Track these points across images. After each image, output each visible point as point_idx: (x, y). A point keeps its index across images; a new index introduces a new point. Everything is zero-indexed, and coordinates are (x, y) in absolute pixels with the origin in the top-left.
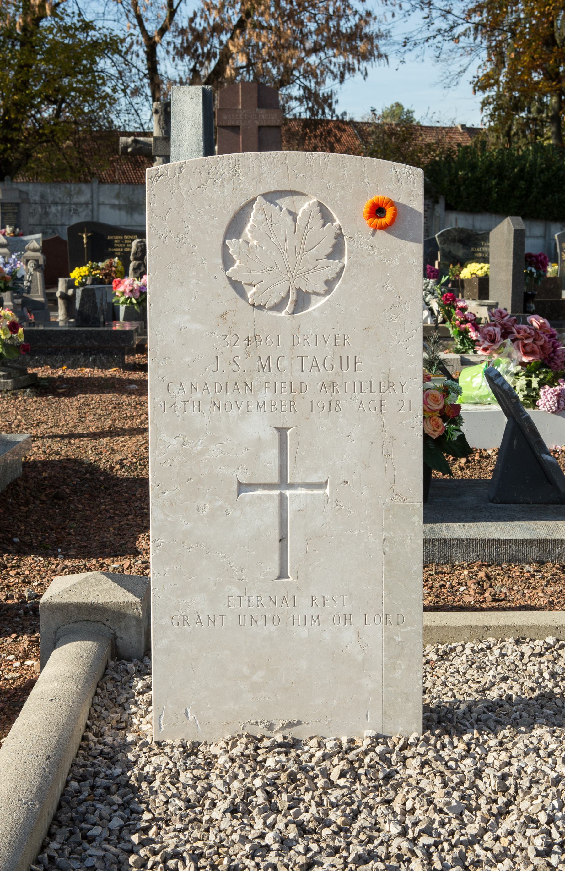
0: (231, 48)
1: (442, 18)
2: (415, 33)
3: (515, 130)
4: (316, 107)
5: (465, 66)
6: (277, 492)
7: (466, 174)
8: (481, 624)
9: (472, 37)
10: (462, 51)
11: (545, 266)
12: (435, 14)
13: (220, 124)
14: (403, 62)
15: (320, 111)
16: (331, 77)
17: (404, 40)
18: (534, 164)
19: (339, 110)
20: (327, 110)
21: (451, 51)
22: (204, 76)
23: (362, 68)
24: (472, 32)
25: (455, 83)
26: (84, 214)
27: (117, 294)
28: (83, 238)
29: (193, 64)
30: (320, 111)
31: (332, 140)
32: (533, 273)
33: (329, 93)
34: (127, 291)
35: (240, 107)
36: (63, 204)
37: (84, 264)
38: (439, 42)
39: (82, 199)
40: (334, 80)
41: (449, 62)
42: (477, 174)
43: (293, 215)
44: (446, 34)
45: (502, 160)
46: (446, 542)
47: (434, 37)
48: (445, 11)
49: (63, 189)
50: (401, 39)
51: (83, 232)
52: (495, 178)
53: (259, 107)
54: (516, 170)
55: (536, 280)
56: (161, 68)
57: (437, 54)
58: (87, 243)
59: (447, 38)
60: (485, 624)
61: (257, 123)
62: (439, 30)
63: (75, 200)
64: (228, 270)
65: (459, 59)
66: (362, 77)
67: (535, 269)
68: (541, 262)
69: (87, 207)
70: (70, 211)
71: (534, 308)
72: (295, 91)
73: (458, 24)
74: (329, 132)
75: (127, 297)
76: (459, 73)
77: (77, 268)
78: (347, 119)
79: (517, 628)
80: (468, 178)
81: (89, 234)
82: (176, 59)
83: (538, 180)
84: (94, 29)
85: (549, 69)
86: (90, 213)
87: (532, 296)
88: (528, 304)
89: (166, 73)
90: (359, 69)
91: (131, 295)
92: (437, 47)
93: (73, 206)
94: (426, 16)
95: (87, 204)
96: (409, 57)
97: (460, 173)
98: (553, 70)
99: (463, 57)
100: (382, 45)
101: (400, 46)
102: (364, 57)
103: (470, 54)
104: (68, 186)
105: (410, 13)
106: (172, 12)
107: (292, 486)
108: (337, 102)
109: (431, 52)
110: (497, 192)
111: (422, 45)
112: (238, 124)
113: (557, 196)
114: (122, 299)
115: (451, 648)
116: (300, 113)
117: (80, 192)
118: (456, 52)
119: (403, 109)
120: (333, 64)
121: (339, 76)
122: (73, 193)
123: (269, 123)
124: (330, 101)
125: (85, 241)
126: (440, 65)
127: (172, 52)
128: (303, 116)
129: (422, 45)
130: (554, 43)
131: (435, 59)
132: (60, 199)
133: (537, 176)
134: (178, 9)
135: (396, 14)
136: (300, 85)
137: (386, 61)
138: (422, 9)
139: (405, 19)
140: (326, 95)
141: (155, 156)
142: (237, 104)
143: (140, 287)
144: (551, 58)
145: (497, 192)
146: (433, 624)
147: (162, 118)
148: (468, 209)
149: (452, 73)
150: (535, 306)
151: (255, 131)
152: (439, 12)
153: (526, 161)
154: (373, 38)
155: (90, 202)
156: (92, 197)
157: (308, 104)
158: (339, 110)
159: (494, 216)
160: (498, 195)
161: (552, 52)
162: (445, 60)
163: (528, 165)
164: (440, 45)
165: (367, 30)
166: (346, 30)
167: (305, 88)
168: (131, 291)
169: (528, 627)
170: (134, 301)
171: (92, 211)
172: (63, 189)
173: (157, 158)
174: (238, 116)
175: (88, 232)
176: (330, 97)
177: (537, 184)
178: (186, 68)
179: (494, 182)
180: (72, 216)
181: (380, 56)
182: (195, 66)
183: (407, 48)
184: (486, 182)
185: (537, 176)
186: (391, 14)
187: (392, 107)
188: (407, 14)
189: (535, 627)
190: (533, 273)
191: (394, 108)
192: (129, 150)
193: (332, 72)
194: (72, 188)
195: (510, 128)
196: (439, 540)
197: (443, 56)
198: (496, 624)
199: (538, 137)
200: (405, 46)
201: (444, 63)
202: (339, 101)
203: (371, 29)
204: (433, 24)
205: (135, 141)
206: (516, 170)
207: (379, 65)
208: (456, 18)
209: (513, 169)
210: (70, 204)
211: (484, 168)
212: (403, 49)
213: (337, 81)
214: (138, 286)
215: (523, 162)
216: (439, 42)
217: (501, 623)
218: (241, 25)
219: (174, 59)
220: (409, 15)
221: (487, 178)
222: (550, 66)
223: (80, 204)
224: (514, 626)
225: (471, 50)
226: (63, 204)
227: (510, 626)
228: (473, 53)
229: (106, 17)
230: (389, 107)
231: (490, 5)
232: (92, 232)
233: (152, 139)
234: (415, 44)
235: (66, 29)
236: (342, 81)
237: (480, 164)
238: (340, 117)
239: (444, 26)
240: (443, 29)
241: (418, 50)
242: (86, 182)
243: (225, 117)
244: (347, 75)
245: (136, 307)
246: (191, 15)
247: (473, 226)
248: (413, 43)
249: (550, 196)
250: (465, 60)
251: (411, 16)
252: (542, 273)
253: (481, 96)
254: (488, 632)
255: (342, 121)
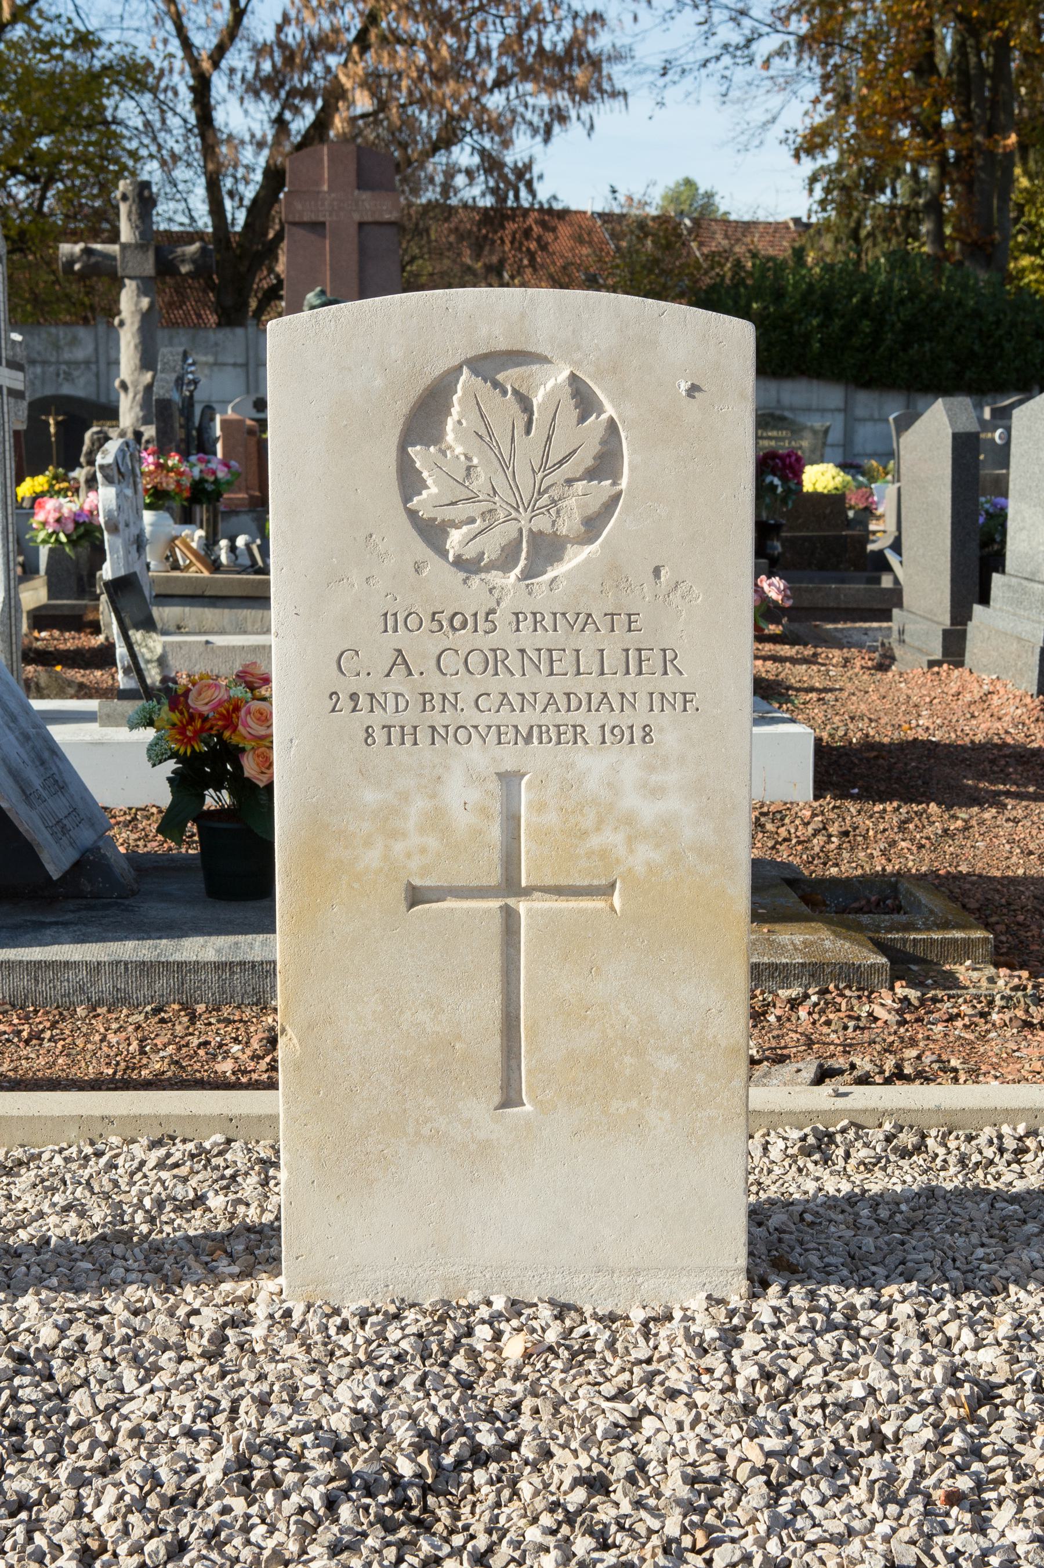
0: (343, 79)
1: (731, 24)
2: (682, 52)
3: (869, 228)
4: (502, 185)
5: (775, 111)
6: (494, 904)
7: (766, 308)
8: (97, 1113)
9: (793, 59)
10: (768, 83)
11: (798, 474)
12: (718, 15)
13: (291, 219)
14: (661, 104)
15: (511, 195)
16: (529, 133)
17: (663, 64)
18: (887, 289)
19: (543, 192)
20: (523, 193)
21: (749, 84)
22: (299, 132)
23: (584, 116)
24: (794, 50)
25: (757, 142)
26: (82, 381)
27: (35, 525)
28: (48, 424)
29: (277, 107)
30: (511, 195)
31: (533, 246)
32: (776, 487)
33: (527, 160)
34: (51, 520)
35: (325, 188)
36: (45, 363)
37: (40, 471)
38: (726, 68)
39: (80, 354)
40: (533, 137)
41: (746, 105)
42: (785, 307)
43: (525, 403)
44: (739, 53)
45: (830, 280)
46: (253, 966)
47: (718, 58)
48: (737, 11)
49: (44, 336)
50: (658, 63)
51: (48, 414)
52: (817, 315)
53: (359, 188)
54: (854, 300)
55: (784, 500)
56: (219, 117)
57: (723, 89)
58: (57, 434)
59: (740, 61)
60: (106, 1113)
61: (357, 217)
62: (726, 46)
63: (66, 356)
64: (411, 500)
65: (764, 98)
66: (585, 132)
67: (780, 478)
68: (791, 467)
69: (88, 368)
70: (58, 375)
71: (780, 549)
72: (463, 155)
73: (760, 35)
74: (527, 233)
75: (50, 530)
76: (765, 124)
77: (28, 479)
78: (557, 206)
79: (160, 1120)
80: (769, 315)
81: (60, 418)
82: (246, 102)
83: (895, 318)
84: (99, 43)
85: (922, 118)
86: (94, 379)
87: (777, 527)
88: (769, 543)
89: (227, 125)
90: (579, 118)
91: (57, 527)
92: (723, 77)
93: (64, 367)
94: (702, 20)
95: (87, 363)
96: (672, 94)
97: (755, 306)
98: (929, 118)
99: (770, 95)
100: (618, 74)
101: (657, 75)
102: (585, 96)
103: (784, 89)
104: (53, 330)
105: (674, 14)
106: (239, 14)
107: (527, 892)
108: (541, 177)
109: (712, 87)
110: (820, 341)
111: (696, 73)
112: (322, 219)
113: (927, 347)
114: (42, 535)
115: (32, 1155)
116: (474, 198)
117: (74, 342)
118: (758, 86)
119: (697, 189)
120: (530, 109)
121: (542, 131)
122: (62, 343)
123: (377, 218)
124: (527, 176)
125: (52, 430)
126: (730, 109)
127: (240, 88)
128: (481, 203)
129: (696, 73)
130: (933, 69)
131: (719, 98)
132: (39, 353)
133: (893, 310)
134: (249, 8)
135: (640, 17)
136: (473, 148)
137: (623, 103)
138: (696, 7)
139: (664, 26)
140: (520, 165)
141: (123, 278)
142: (318, 182)
143: (75, 514)
144: (925, 97)
145: (820, 341)
146: (15, 1113)
147: (134, 208)
148: (769, 370)
149: (752, 125)
150: (783, 546)
151: (353, 230)
152: (726, 12)
153: (874, 284)
154: (600, 61)
155: (93, 359)
156: (96, 350)
157: (487, 182)
158: (543, 192)
159: (815, 382)
160: (823, 345)
161: (929, 85)
162: (739, 101)
163: (876, 290)
164: (727, 73)
165: (592, 45)
166: (555, 45)
167: (483, 153)
168: (58, 521)
169: (179, 1117)
170: (63, 538)
171: (97, 375)
172: (44, 336)
173: (127, 281)
174: (323, 205)
175: (57, 414)
176: (528, 167)
177: (893, 325)
178: (265, 118)
179: (815, 322)
180: (61, 385)
181: (614, 94)
182: (280, 115)
183: (668, 78)
184: (800, 322)
185: (893, 310)
186: (631, 17)
187: (678, 185)
188: (667, 16)
189: (193, 1118)
190: (776, 487)
191: (682, 188)
192: (77, 267)
193: (531, 124)
194: (61, 334)
195: (859, 224)
196: (243, 963)
197: (734, 94)
198: (125, 1113)
199: (910, 240)
200: (664, 75)
201: (737, 107)
202: (545, 177)
203: (599, 43)
204: (714, 34)
205: (87, 251)
206: (854, 300)
207: (612, 111)
208: (757, 25)
209: (850, 297)
210: (58, 363)
211: (798, 297)
212: (661, 82)
213: (539, 139)
214: (70, 511)
215: (868, 286)
216: (726, 68)
217: (135, 1111)
218: (362, 40)
219: (242, 99)
220: (672, 18)
221: (803, 315)
222: (923, 110)
223: (76, 364)
224: (156, 1116)
225: (787, 83)
226: (45, 363)
227: (149, 1117)
228: (789, 89)
229: (125, 25)
230: (672, 185)
231: (822, 1)
232: (64, 414)
233: (116, 248)
234: (683, 71)
235: (46, 47)
236: (547, 139)
237: (790, 289)
238: (546, 206)
239: (736, 38)
240: (734, 43)
241: (688, 83)
242: (86, 321)
243: (299, 207)
244: (556, 128)
245: (67, 549)
246: (279, 20)
247: (779, 401)
248: (679, 69)
249: (916, 346)
250: (775, 101)
251: (676, 21)
252: (793, 486)
253: (808, 166)
254: (111, 1127)
255: (550, 211)
